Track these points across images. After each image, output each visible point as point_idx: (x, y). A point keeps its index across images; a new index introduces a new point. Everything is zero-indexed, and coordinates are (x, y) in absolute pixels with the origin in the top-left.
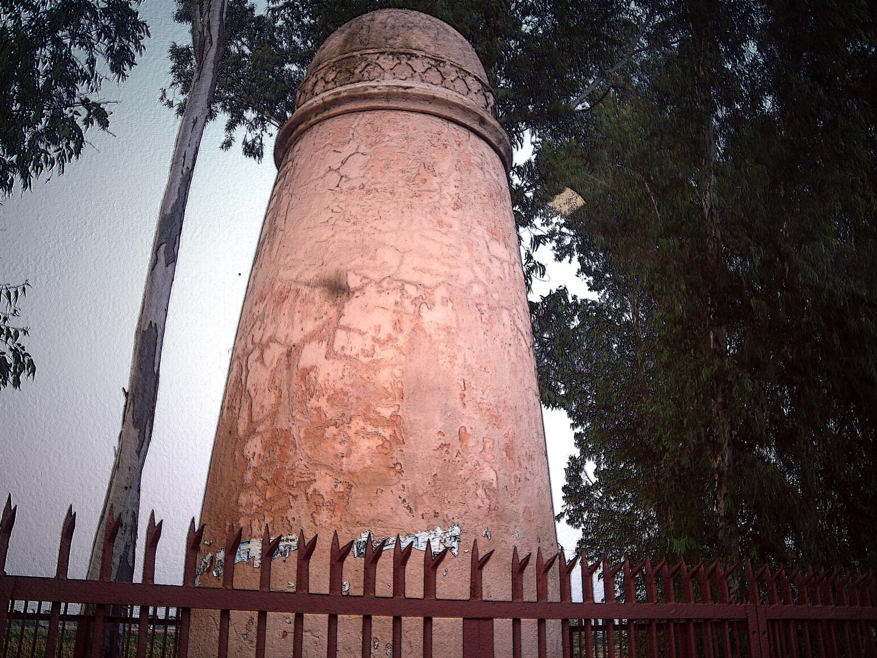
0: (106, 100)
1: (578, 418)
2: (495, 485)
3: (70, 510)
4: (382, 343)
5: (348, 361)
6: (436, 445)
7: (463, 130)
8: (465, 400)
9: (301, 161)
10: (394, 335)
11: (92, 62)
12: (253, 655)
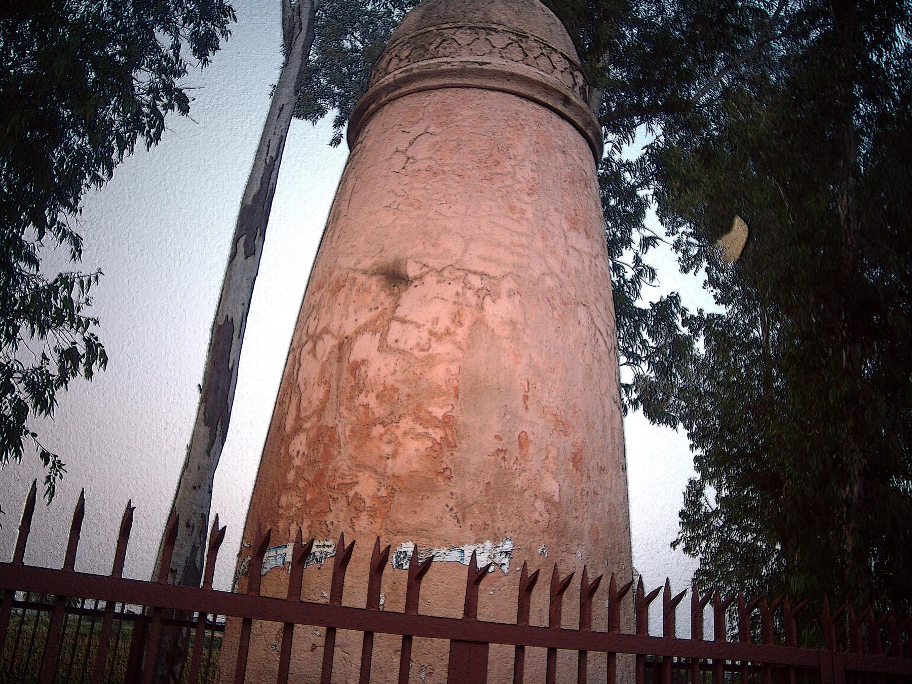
0: (192, 85)
1: (697, 439)
2: (556, 498)
3: (129, 504)
4: (439, 338)
5: (402, 356)
6: (493, 450)
7: (543, 110)
8: (529, 403)
9: (369, 143)
10: (452, 329)
11: (176, 47)
12: (394, 676)
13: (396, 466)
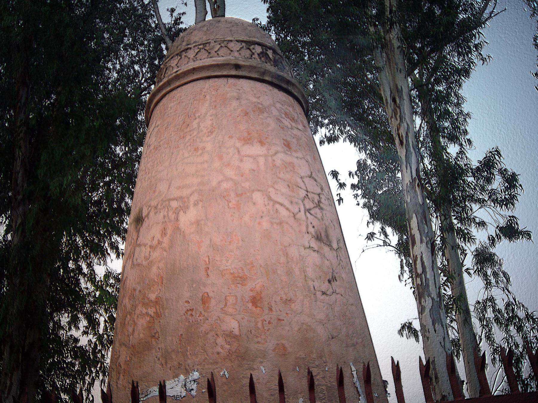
3: (309, 369)
13: (133, 340)
